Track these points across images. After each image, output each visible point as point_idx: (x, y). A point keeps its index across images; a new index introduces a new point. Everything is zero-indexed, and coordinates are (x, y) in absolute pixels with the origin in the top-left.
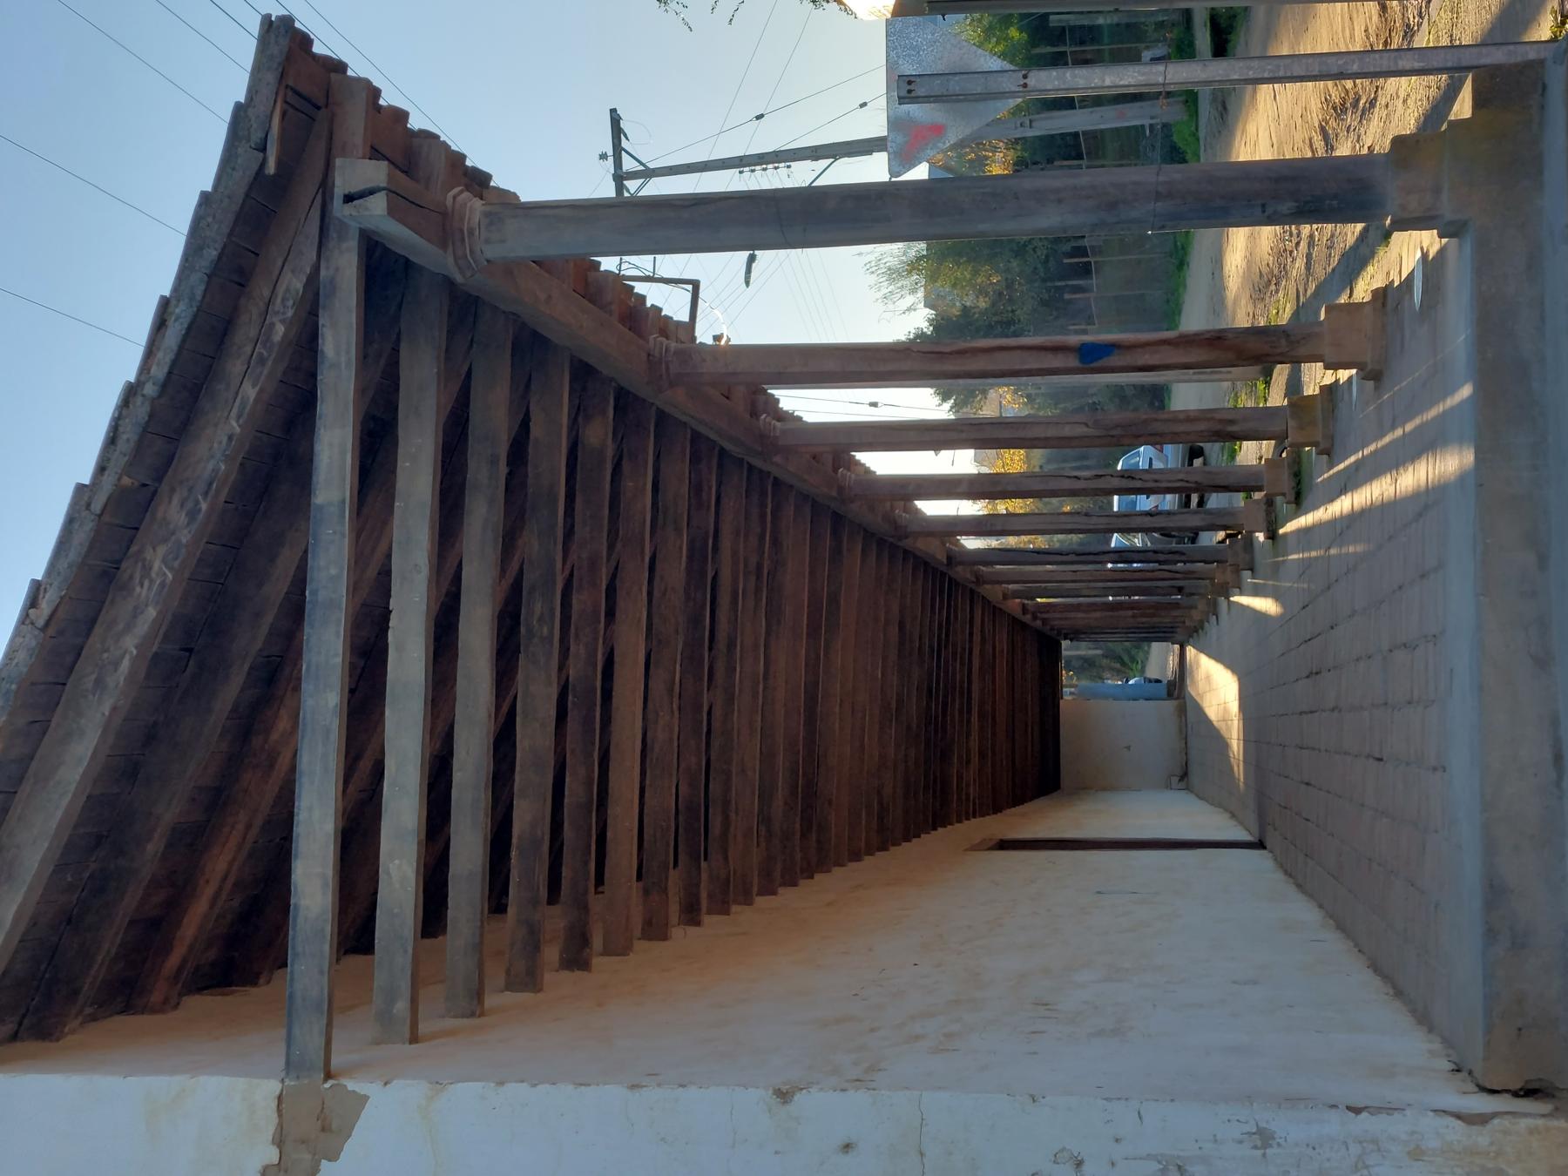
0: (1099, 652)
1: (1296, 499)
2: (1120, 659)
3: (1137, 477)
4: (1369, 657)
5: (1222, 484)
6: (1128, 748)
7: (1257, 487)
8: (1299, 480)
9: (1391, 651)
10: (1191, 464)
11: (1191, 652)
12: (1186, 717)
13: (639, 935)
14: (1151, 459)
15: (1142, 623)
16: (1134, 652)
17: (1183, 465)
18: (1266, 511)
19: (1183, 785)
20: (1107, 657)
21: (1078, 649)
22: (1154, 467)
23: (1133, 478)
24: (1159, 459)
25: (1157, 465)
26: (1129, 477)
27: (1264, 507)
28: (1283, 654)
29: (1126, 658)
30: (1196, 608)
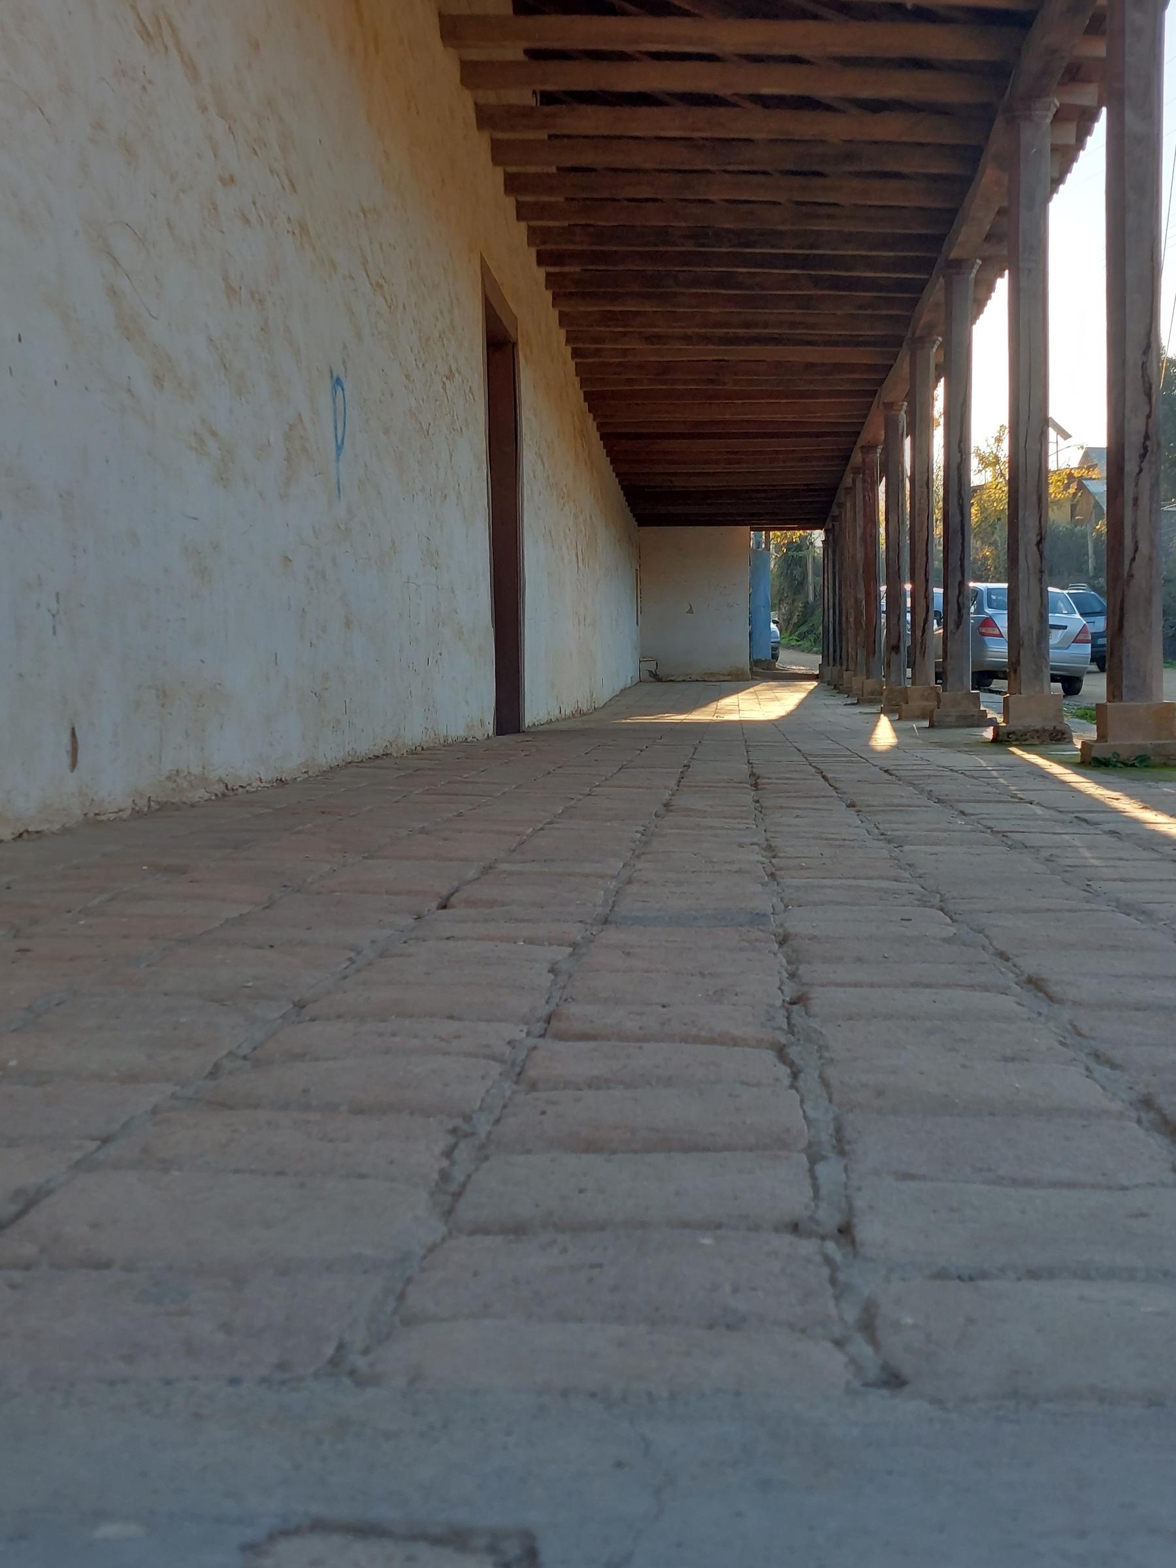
0: (811, 598)
1: (1096, 759)
2: (803, 621)
3: (1145, 465)
4: (772, 876)
5: (1125, 624)
6: (691, 611)
7: (1120, 688)
8: (1133, 765)
9: (783, 941)
10: (1054, 679)
11: (811, 685)
12: (730, 681)
13: (547, 271)
14: (1065, 627)
15: (847, 618)
16: (811, 637)
17: (1053, 668)
18: (1044, 730)
19: (646, 675)
20: (805, 607)
21: (815, 574)
22: (1054, 632)
23: (1143, 456)
24: (1064, 639)
25: (1055, 637)
26: (1145, 448)
27: (1049, 726)
28: (799, 750)
29: (804, 629)
30: (867, 678)
